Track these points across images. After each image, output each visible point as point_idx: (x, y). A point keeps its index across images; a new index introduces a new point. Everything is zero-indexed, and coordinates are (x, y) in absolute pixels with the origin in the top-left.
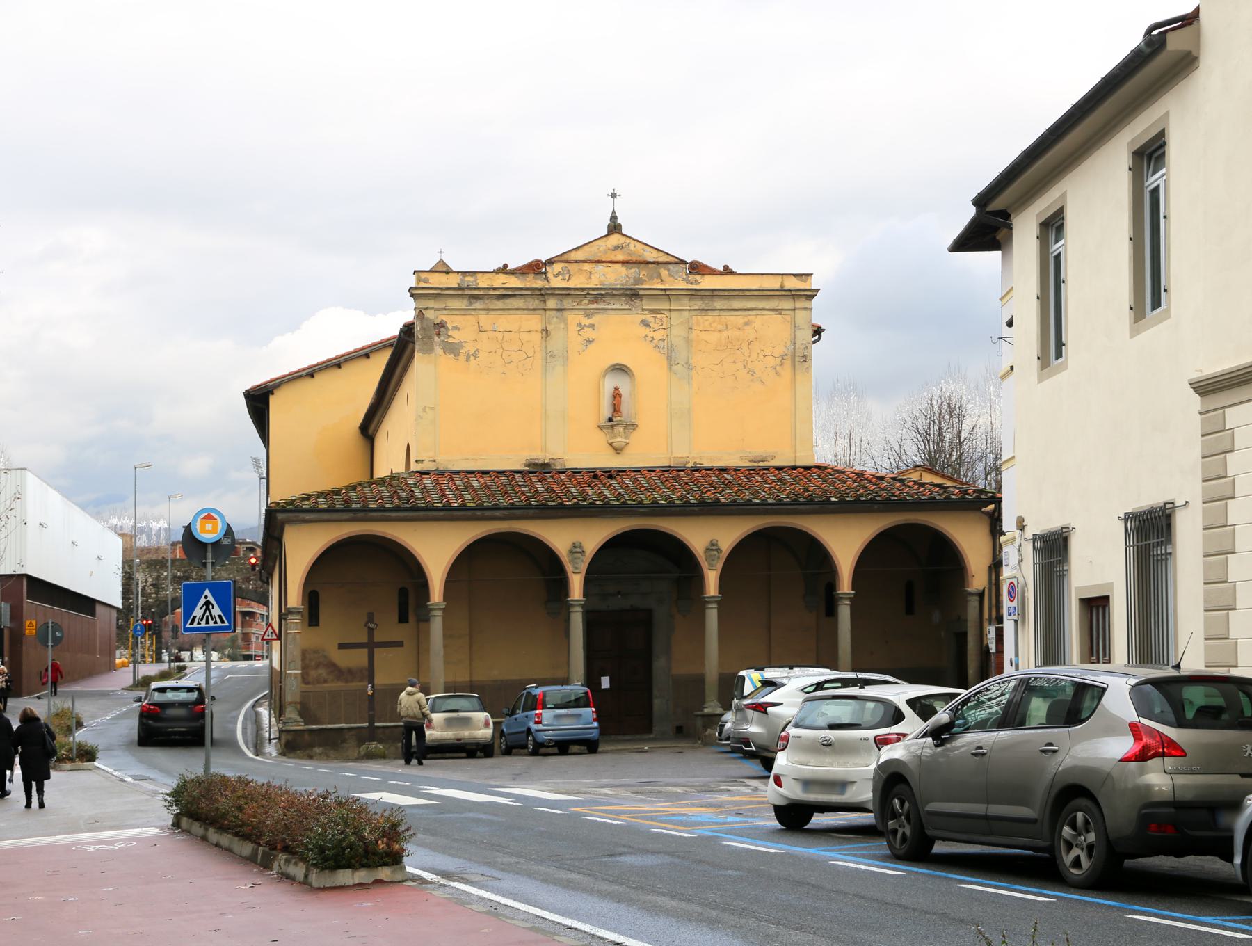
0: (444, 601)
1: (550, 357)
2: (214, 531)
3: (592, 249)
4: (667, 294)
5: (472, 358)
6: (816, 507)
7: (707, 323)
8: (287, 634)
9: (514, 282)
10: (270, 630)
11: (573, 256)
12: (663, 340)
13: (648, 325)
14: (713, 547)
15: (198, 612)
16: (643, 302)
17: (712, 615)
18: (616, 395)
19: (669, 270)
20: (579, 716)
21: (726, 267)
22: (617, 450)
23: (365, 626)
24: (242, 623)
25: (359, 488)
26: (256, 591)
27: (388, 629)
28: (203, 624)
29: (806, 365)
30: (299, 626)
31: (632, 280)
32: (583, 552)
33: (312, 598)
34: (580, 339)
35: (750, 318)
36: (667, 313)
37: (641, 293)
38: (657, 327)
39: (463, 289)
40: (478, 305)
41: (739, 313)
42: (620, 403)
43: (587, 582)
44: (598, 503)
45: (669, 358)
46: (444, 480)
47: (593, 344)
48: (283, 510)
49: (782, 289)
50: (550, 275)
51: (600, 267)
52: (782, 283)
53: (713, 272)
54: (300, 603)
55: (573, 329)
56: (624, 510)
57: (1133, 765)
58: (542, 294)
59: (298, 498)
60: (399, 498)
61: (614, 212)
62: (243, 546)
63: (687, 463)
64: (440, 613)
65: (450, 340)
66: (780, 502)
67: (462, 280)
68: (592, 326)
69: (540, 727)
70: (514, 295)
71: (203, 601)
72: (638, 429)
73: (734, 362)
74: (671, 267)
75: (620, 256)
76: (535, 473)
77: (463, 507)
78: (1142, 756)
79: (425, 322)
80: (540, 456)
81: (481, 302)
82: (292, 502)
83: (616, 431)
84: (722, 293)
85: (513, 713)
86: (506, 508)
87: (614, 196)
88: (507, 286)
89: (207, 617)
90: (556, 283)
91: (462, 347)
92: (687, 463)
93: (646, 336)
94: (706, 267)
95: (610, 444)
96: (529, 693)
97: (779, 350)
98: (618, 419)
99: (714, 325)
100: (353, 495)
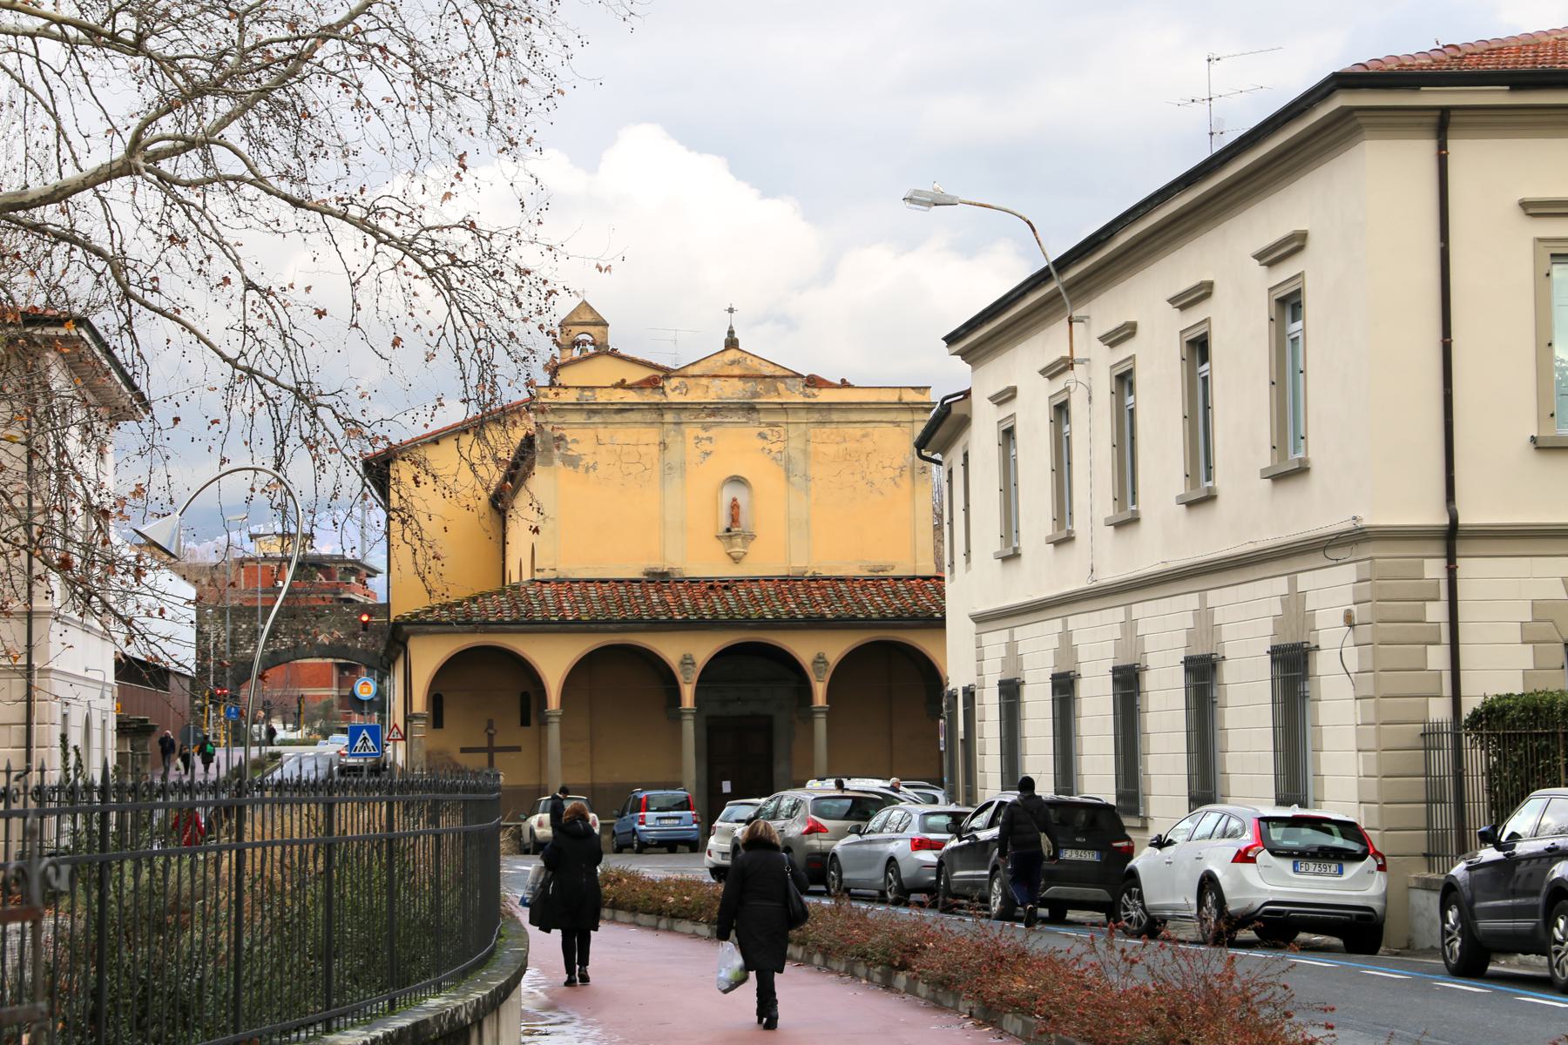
0: (561, 708)
1: (668, 469)
2: (369, 693)
3: (709, 364)
4: (784, 408)
5: (591, 470)
6: (921, 622)
7: (824, 436)
8: (412, 738)
9: (632, 397)
10: (395, 730)
11: (691, 371)
12: (780, 452)
13: (765, 438)
14: (820, 660)
15: (359, 744)
16: (761, 415)
17: (821, 725)
18: (734, 506)
19: (786, 384)
20: (679, 818)
21: (843, 381)
22: (736, 560)
23: (486, 731)
24: (339, 679)
25: (480, 600)
26: (366, 650)
27: (510, 733)
28: (362, 752)
29: (925, 476)
30: (424, 730)
31: (749, 394)
32: (693, 664)
33: (436, 701)
34: (698, 452)
35: (870, 430)
36: (785, 426)
37: (758, 407)
38: (774, 439)
39: (581, 404)
40: (596, 419)
41: (857, 425)
42: (738, 514)
43: (698, 690)
44: (707, 617)
45: (787, 470)
46: (563, 589)
47: (711, 457)
48: (408, 623)
49: (900, 402)
50: (667, 390)
51: (717, 382)
52: (900, 396)
53: (830, 385)
54: (425, 708)
55: (691, 441)
56: (731, 624)
57: (806, 836)
58: (660, 408)
59: (422, 611)
60: (519, 611)
61: (731, 327)
62: (339, 565)
63: (806, 572)
64: (557, 720)
65: (569, 453)
66: (884, 618)
67: (581, 395)
68: (710, 439)
69: (643, 827)
70: (632, 410)
71: (362, 737)
72: (756, 539)
73: (853, 474)
74: (788, 381)
75: (737, 371)
76: (653, 582)
77: (578, 621)
78: (810, 831)
79: (544, 436)
80: (659, 565)
81: (600, 416)
82: (417, 615)
83: (734, 541)
84: (839, 407)
85: (622, 815)
86: (618, 622)
87: (731, 310)
88: (625, 400)
89: (365, 747)
90: (674, 397)
91: (582, 459)
92: (806, 572)
93: (764, 449)
94: (823, 380)
95: (729, 554)
96: (635, 797)
97: (898, 463)
98: (736, 529)
99: (833, 437)
100: (474, 607)
